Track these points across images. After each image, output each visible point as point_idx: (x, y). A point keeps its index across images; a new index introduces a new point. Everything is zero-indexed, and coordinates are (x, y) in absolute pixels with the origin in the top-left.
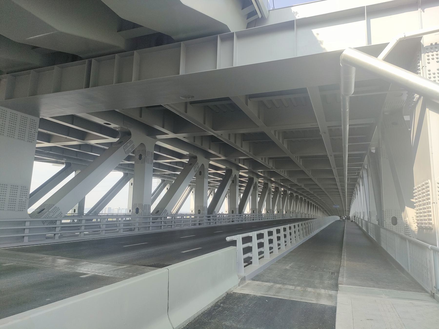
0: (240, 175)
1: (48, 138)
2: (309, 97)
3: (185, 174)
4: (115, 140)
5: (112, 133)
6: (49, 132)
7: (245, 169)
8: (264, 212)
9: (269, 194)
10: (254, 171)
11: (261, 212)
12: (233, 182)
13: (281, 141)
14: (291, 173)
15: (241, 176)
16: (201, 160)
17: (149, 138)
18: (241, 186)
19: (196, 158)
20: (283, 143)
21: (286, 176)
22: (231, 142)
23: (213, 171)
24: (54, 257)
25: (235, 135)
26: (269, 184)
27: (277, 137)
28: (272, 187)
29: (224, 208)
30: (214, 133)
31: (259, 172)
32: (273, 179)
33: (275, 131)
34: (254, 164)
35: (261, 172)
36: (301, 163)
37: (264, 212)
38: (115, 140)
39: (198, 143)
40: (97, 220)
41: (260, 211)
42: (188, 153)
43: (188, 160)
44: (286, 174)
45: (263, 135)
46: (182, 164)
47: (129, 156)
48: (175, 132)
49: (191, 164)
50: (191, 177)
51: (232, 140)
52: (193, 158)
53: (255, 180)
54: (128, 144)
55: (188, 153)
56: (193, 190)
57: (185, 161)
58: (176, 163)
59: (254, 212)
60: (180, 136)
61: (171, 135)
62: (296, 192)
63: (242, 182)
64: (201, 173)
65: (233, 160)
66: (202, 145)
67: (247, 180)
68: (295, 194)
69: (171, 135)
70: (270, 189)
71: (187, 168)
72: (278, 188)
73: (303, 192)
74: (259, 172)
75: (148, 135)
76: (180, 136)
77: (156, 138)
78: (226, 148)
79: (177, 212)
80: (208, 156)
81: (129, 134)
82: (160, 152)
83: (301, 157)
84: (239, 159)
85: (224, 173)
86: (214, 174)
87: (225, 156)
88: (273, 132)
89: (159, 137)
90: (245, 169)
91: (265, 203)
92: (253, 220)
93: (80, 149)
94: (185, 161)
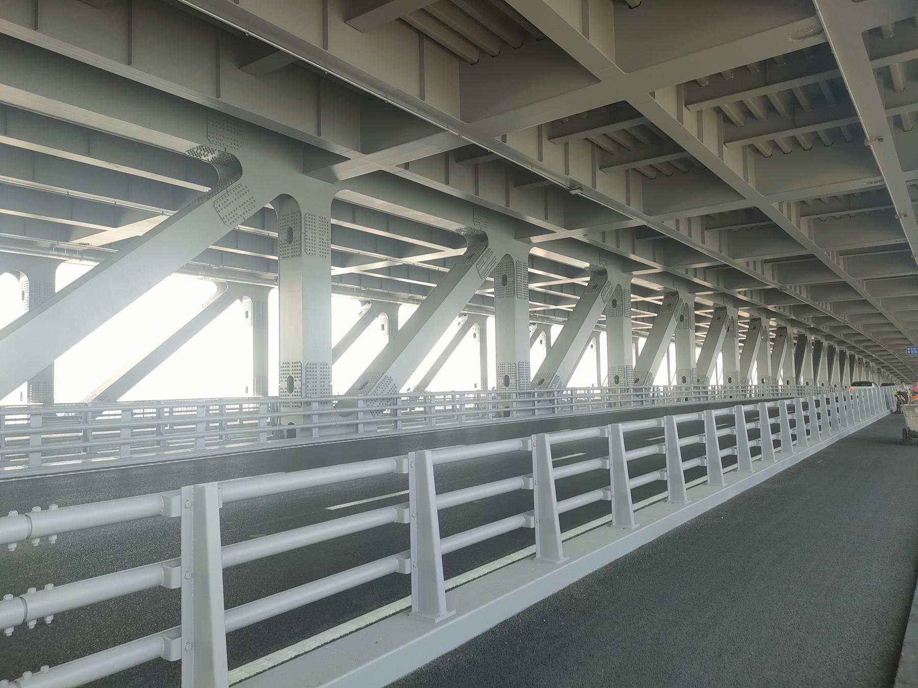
0: (696, 303)
1: (342, 259)
2: (841, 78)
3: (583, 309)
4: (462, 251)
5: (452, 239)
6: (120, 202)
7: (708, 289)
8: (754, 380)
9: (764, 341)
10: (728, 291)
11: (707, 380)
12: (682, 318)
13: (794, 222)
14: (817, 290)
15: (698, 306)
16: (615, 275)
17: (518, 243)
18: (698, 329)
19: (603, 273)
20: (799, 226)
21: (804, 298)
22: (682, 235)
23: (565, 280)
24: (165, 494)
25: (689, 219)
26: (763, 319)
27: (785, 215)
28: (771, 327)
29: (716, 378)
30: (647, 220)
31: (739, 293)
32: (771, 308)
33: (780, 204)
34: (728, 275)
35: (745, 294)
36: (842, 267)
37: (754, 380)
38: (462, 251)
39: (610, 245)
40: (171, 412)
41: (745, 380)
42: (588, 265)
43: (588, 279)
44: (804, 295)
45: (753, 215)
46: (574, 288)
47: (236, 233)
48: (568, 227)
49: (595, 287)
50: (597, 313)
51: (683, 230)
52: (599, 276)
53: (731, 311)
54: (485, 259)
55: (588, 265)
56: (591, 343)
57: (583, 281)
58: (561, 288)
59: (617, 382)
60: (577, 234)
61: (562, 234)
62: (813, 330)
63: (699, 319)
64: (616, 305)
65: (680, 271)
66: (604, 241)
67: (711, 313)
68: (793, 331)
69: (562, 234)
70: (766, 334)
71: (587, 295)
72: (785, 328)
73: (835, 328)
74: (739, 293)
75: (517, 238)
76: (577, 234)
77: (530, 242)
78: (668, 248)
79: (421, 387)
80: (630, 266)
81: (482, 239)
82: (354, 222)
83: (842, 253)
84: (695, 269)
85: (660, 300)
86: (637, 305)
87: (665, 263)
88: (775, 205)
89: (535, 239)
90: (708, 289)
91: (719, 359)
92: (686, 399)
93: (389, 275)
94: (583, 281)
